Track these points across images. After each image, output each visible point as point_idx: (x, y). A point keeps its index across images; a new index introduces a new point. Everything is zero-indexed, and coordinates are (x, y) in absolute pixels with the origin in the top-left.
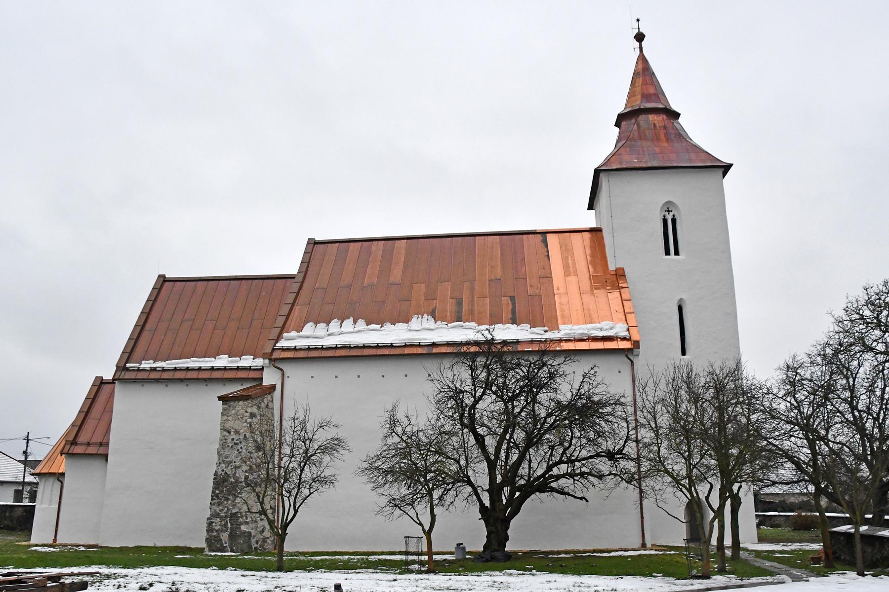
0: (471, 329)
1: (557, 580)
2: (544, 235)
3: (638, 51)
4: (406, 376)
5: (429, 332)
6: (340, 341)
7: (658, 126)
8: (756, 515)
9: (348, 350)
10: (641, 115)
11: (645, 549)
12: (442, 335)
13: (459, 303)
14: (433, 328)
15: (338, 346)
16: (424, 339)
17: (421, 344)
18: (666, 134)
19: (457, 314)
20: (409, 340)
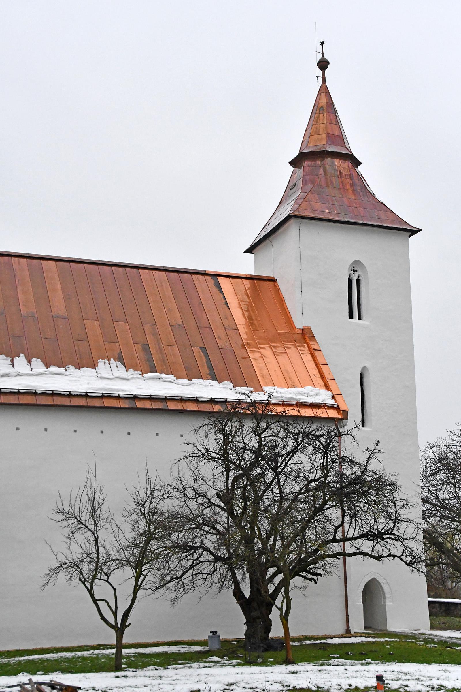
0: (170, 382)
1: (274, 671)
2: (215, 277)
3: (320, 79)
4: (129, 433)
5: (125, 382)
6: (20, 384)
7: (343, 173)
8: (430, 602)
9: (34, 397)
10: (327, 158)
11: (350, 635)
12: (141, 387)
13: (146, 349)
14: (129, 378)
15: (21, 391)
16: (123, 390)
17: (121, 396)
18: (352, 185)
19: (147, 363)
20: (105, 390)
